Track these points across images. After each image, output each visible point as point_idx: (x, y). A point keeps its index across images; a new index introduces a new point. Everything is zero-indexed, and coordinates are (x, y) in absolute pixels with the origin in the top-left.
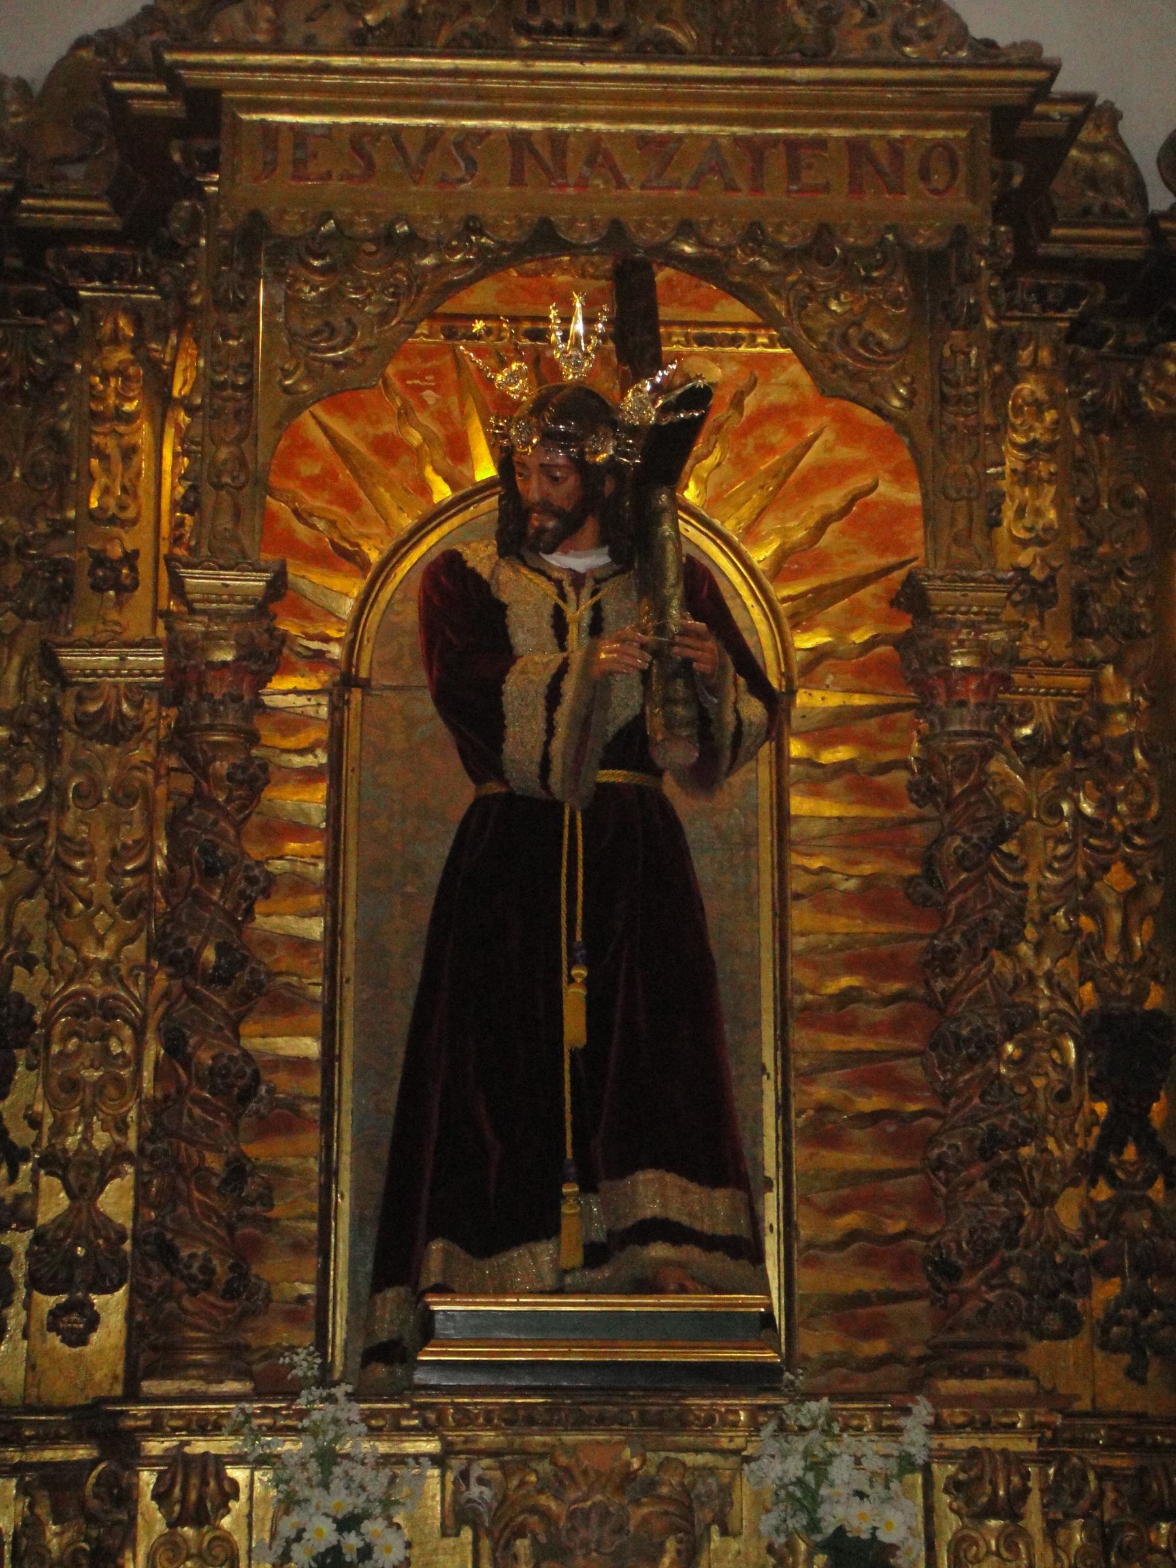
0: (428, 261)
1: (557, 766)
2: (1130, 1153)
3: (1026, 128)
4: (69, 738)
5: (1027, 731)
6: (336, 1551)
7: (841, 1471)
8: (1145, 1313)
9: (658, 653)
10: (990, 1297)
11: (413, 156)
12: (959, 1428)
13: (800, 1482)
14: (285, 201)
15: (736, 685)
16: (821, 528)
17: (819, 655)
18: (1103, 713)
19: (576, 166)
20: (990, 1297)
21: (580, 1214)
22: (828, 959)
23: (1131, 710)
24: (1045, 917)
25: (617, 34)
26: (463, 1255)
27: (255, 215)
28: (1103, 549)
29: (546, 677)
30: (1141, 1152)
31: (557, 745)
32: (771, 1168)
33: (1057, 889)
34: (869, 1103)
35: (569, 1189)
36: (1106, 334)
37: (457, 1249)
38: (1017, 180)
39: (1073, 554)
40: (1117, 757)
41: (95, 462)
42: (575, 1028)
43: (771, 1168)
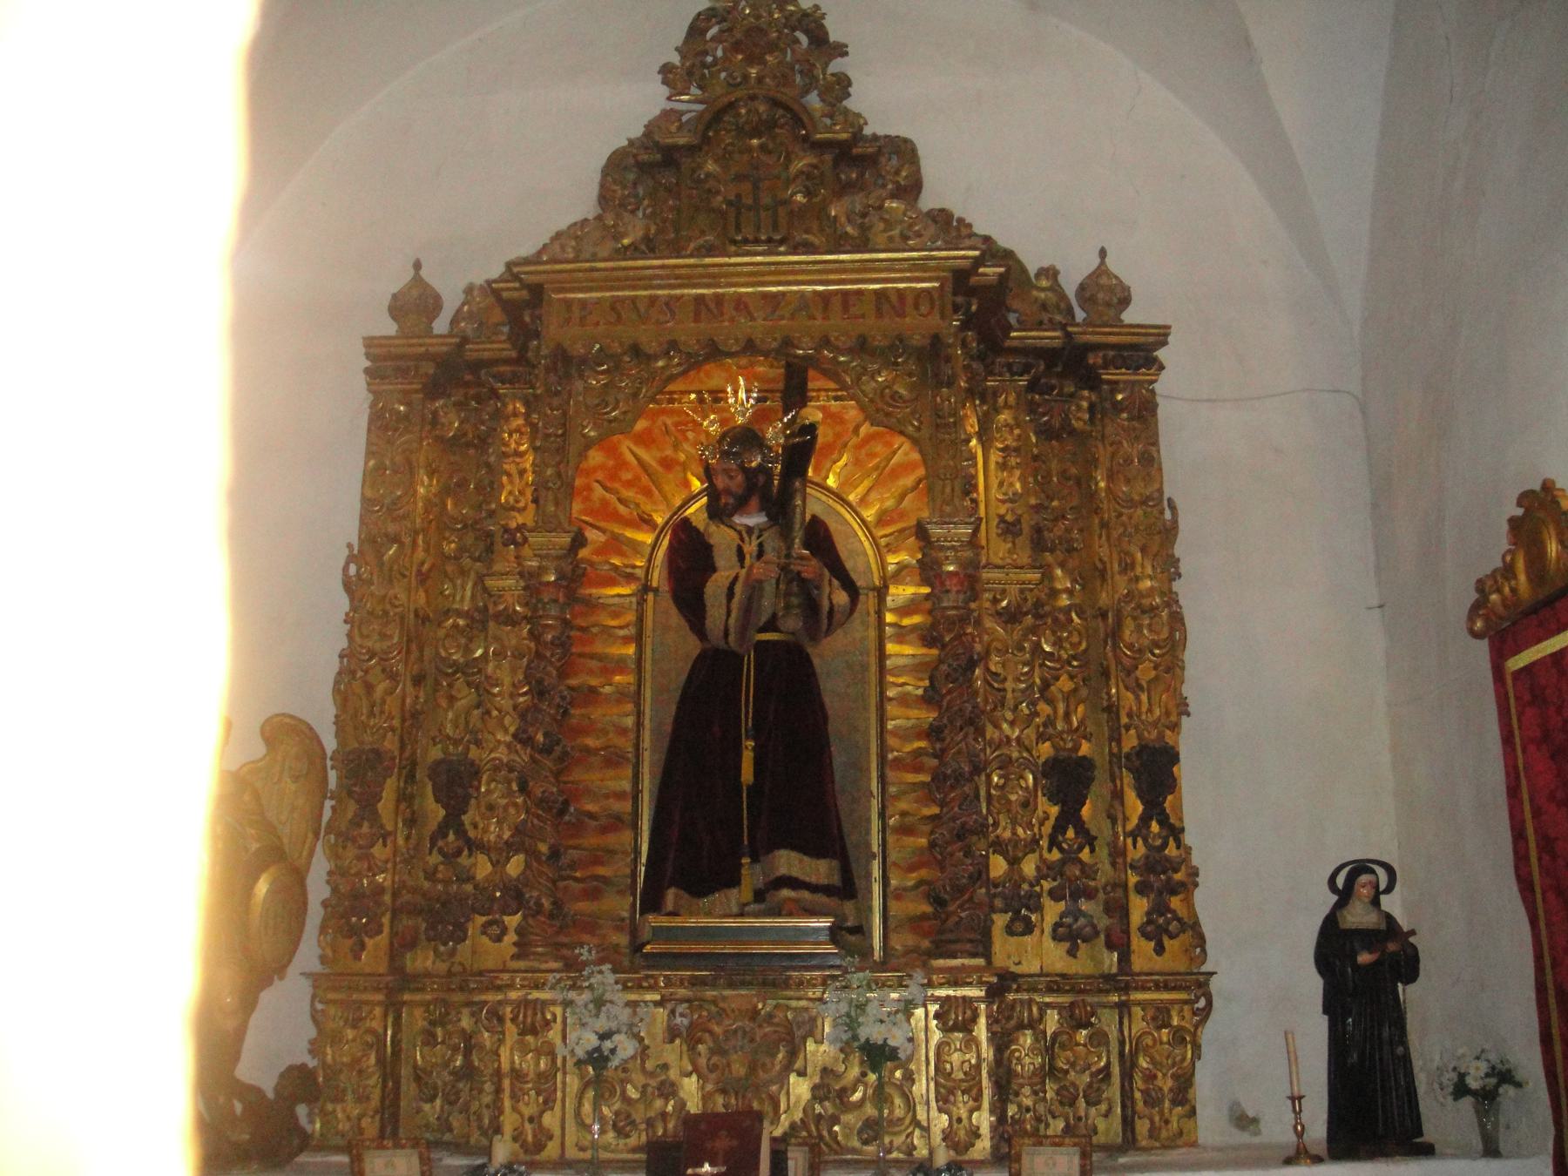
0: (660, 364)
1: (732, 630)
2: (1070, 833)
3: (974, 280)
4: (491, 624)
5: (1005, 603)
6: (598, 1049)
7: (872, 1009)
8: (1076, 920)
9: (784, 569)
10: (963, 915)
11: (642, 310)
12: (941, 985)
13: (848, 1015)
14: (575, 339)
15: (830, 584)
16: (902, 497)
17: (902, 567)
18: (1054, 593)
19: (729, 309)
20: (963, 915)
21: (751, 876)
22: (904, 735)
23: (1070, 592)
24: (1016, 707)
25: (782, 242)
26: (686, 896)
27: (559, 346)
28: (1055, 503)
29: (727, 583)
30: (1077, 833)
31: (732, 621)
32: (875, 848)
33: (1023, 691)
34: (927, 811)
35: (746, 860)
36: (1053, 388)
37: (682, 892)
38: (974, 308)
39: (1033, 507)
40: (1062, 617)
41: (505, 478)
42: (747, 774)
43: (875, 848)
